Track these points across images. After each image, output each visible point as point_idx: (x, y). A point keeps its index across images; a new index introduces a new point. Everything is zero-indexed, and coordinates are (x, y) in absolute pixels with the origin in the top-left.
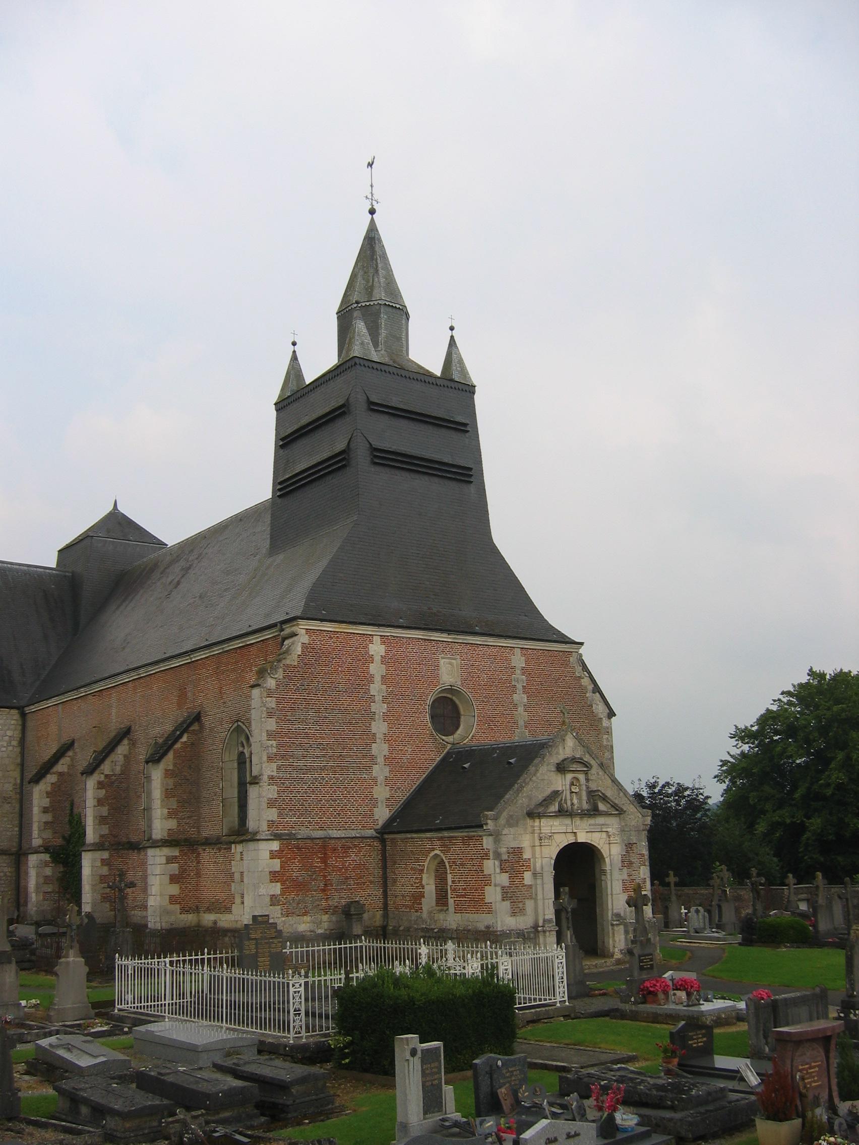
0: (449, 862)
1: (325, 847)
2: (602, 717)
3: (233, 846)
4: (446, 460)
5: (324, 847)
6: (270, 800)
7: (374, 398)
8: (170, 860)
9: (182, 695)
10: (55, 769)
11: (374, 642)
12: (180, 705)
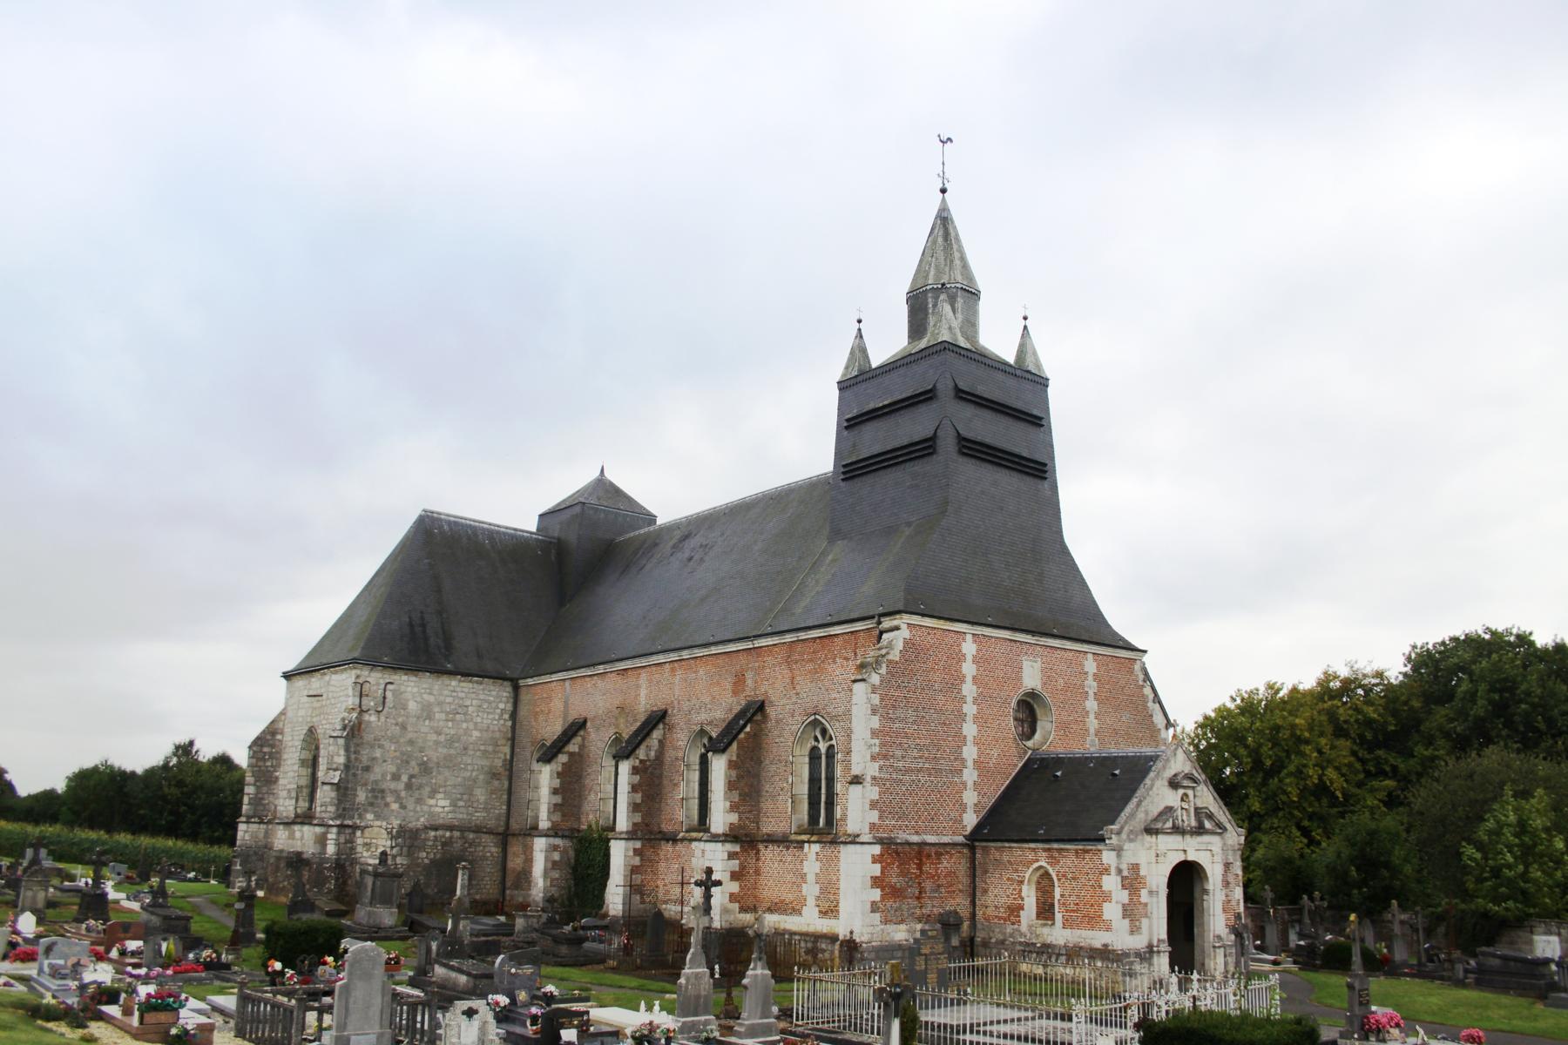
0: (1057, 875)
1: (921, 852)
3: (806, 845)
4: (1025, 455)
5: (920, 853)
6: (872, 801)
7: (962, 386)
8: (731, 856)
9: (739, 681)
10: (566, 749)
12: (735, 693)
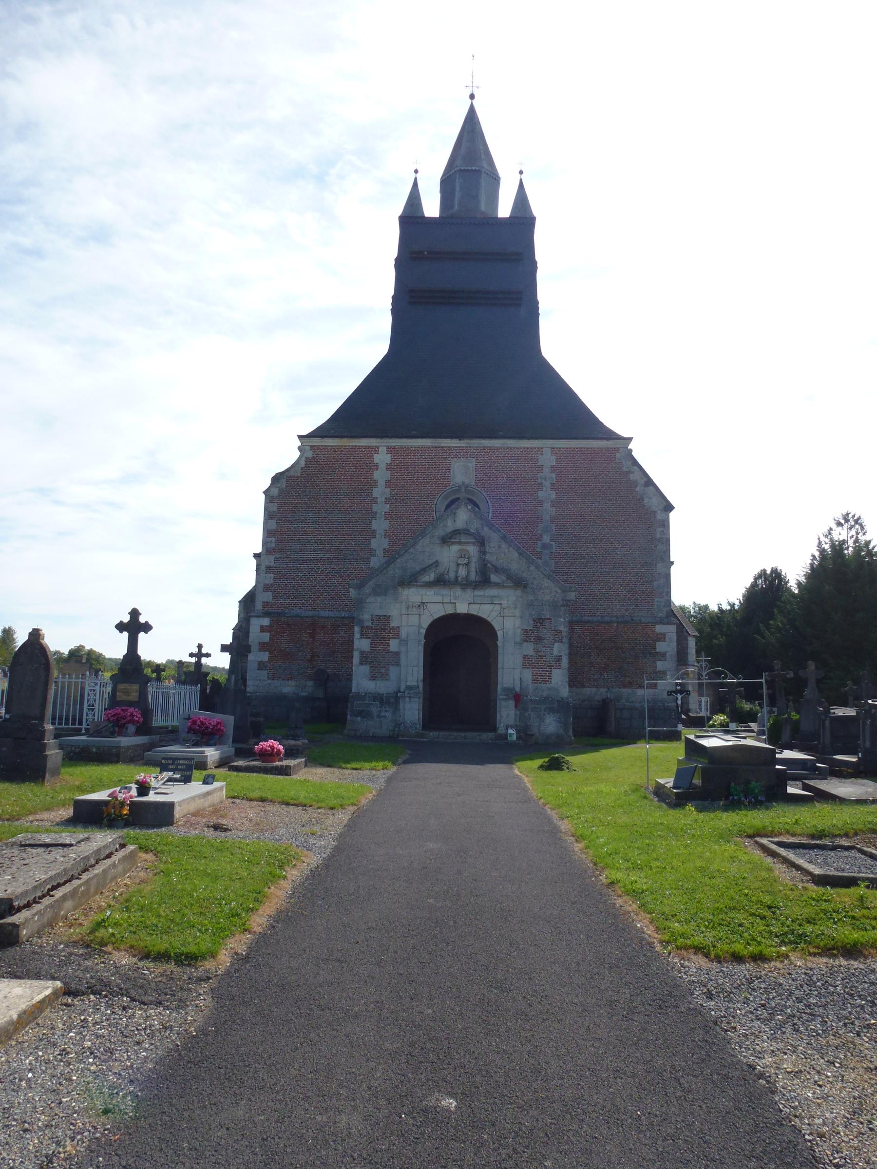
2: (655, 510)
11: (380, 452)
